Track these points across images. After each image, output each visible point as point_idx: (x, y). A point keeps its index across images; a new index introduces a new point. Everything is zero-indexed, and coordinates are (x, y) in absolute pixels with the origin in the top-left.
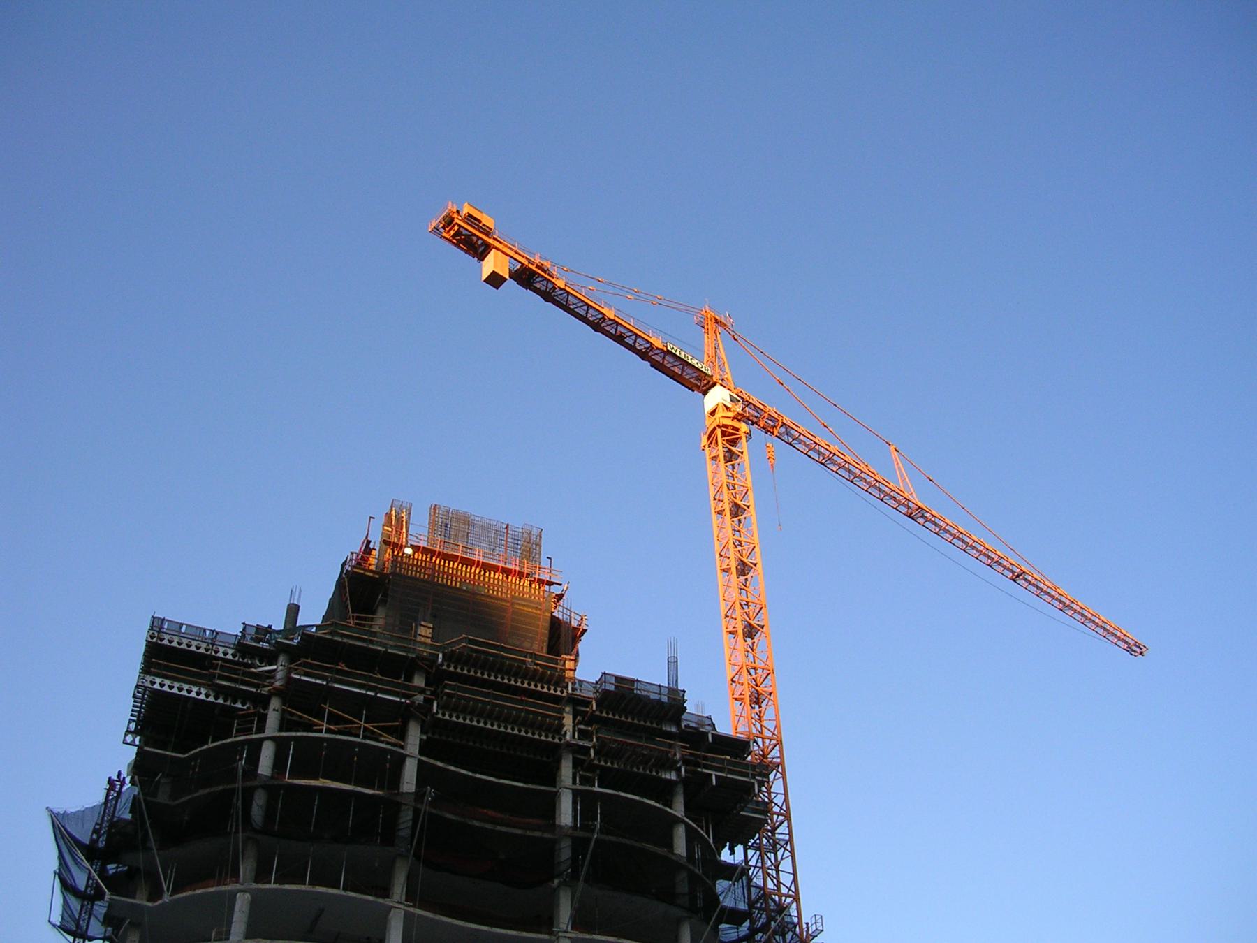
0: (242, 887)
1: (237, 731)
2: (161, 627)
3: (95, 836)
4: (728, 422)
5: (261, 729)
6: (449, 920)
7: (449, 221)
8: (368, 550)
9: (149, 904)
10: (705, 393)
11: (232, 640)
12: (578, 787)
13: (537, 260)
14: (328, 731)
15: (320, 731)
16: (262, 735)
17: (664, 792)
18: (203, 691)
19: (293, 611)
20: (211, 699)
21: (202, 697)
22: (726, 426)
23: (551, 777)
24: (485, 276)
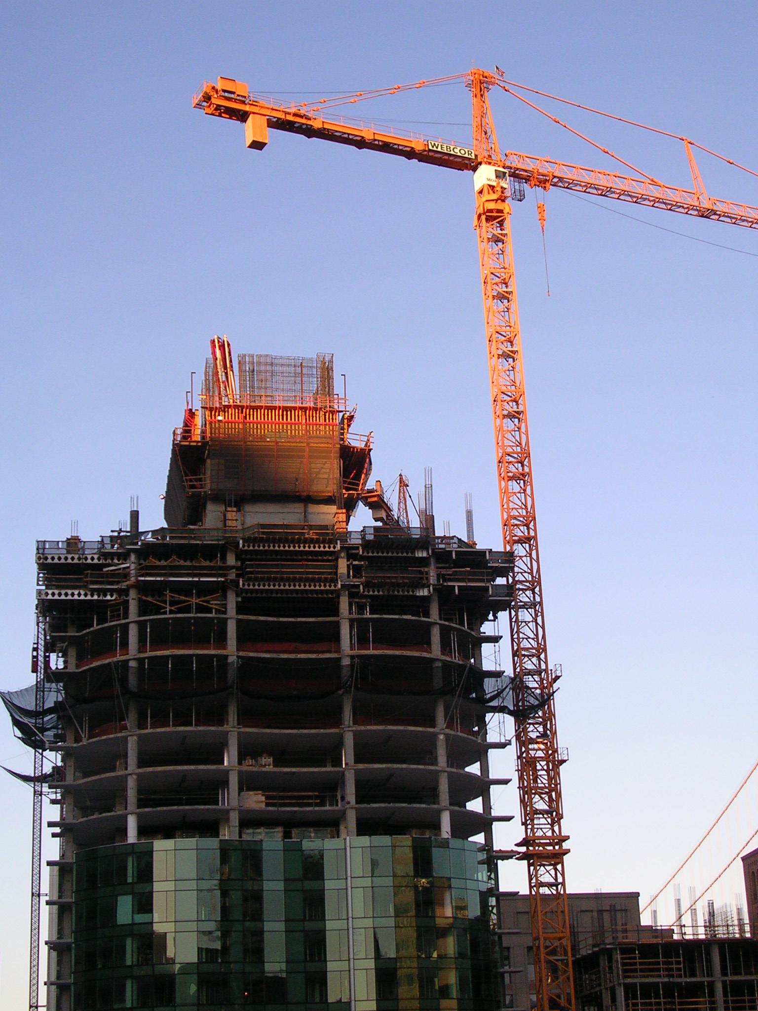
0: (129, 733)
1: (112, 617)
2: (44, 549)
3: (35, 654)
4: (491, 206)
5: (126, 615)
6: (268, 731)
7: (207, 98)
8: (191, 414)
9: (75, 745)
10: (475, 169)
11: (96, 546)
12: (355, 616)
13: (293, 110)
14: (171, 612)
15: (165, 613)
16: (127, 621)
17: (422, 606)
18: (82, 592)
19: (135, 516)
20: (89, 597)
21: (82, 597)
22: (491, 211)
23: (336, 612)
24: (248, 143)
